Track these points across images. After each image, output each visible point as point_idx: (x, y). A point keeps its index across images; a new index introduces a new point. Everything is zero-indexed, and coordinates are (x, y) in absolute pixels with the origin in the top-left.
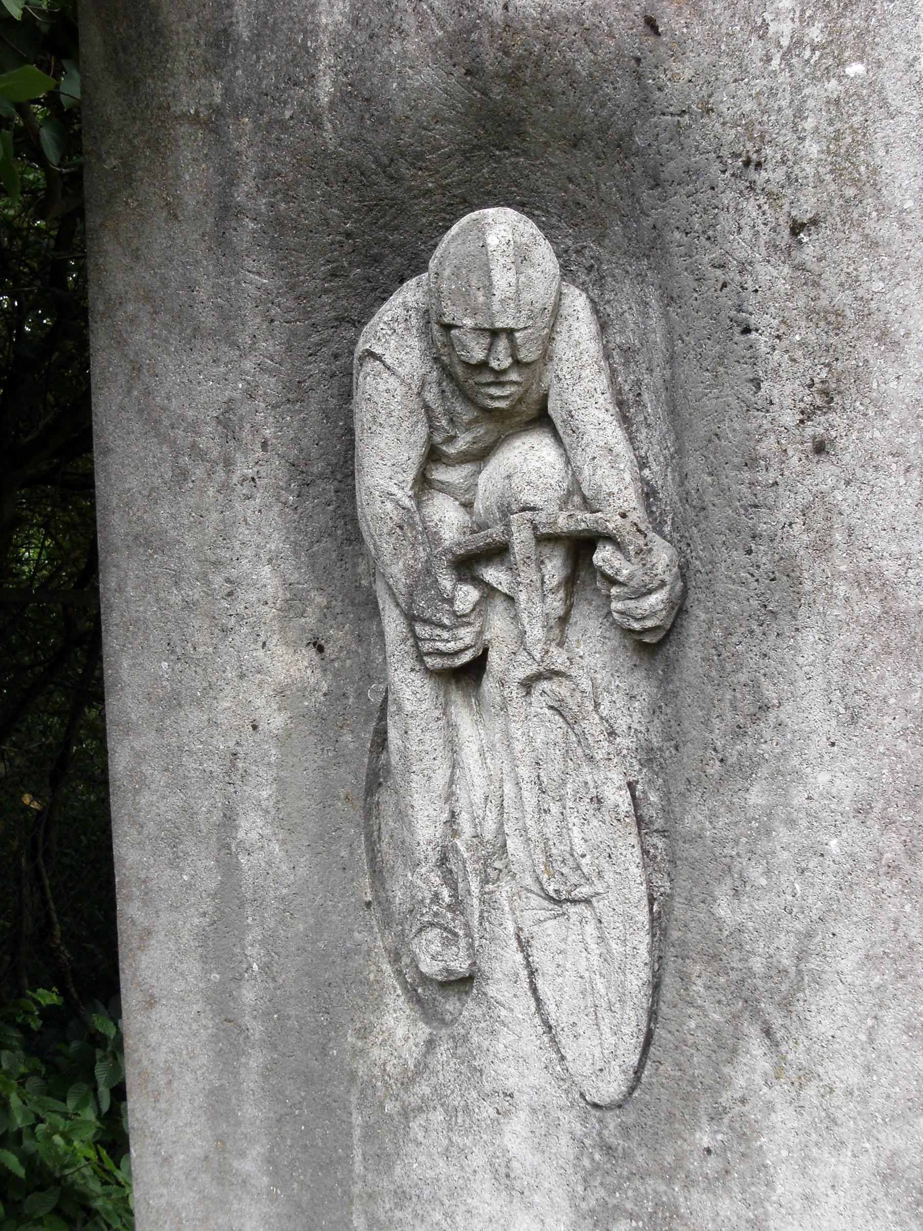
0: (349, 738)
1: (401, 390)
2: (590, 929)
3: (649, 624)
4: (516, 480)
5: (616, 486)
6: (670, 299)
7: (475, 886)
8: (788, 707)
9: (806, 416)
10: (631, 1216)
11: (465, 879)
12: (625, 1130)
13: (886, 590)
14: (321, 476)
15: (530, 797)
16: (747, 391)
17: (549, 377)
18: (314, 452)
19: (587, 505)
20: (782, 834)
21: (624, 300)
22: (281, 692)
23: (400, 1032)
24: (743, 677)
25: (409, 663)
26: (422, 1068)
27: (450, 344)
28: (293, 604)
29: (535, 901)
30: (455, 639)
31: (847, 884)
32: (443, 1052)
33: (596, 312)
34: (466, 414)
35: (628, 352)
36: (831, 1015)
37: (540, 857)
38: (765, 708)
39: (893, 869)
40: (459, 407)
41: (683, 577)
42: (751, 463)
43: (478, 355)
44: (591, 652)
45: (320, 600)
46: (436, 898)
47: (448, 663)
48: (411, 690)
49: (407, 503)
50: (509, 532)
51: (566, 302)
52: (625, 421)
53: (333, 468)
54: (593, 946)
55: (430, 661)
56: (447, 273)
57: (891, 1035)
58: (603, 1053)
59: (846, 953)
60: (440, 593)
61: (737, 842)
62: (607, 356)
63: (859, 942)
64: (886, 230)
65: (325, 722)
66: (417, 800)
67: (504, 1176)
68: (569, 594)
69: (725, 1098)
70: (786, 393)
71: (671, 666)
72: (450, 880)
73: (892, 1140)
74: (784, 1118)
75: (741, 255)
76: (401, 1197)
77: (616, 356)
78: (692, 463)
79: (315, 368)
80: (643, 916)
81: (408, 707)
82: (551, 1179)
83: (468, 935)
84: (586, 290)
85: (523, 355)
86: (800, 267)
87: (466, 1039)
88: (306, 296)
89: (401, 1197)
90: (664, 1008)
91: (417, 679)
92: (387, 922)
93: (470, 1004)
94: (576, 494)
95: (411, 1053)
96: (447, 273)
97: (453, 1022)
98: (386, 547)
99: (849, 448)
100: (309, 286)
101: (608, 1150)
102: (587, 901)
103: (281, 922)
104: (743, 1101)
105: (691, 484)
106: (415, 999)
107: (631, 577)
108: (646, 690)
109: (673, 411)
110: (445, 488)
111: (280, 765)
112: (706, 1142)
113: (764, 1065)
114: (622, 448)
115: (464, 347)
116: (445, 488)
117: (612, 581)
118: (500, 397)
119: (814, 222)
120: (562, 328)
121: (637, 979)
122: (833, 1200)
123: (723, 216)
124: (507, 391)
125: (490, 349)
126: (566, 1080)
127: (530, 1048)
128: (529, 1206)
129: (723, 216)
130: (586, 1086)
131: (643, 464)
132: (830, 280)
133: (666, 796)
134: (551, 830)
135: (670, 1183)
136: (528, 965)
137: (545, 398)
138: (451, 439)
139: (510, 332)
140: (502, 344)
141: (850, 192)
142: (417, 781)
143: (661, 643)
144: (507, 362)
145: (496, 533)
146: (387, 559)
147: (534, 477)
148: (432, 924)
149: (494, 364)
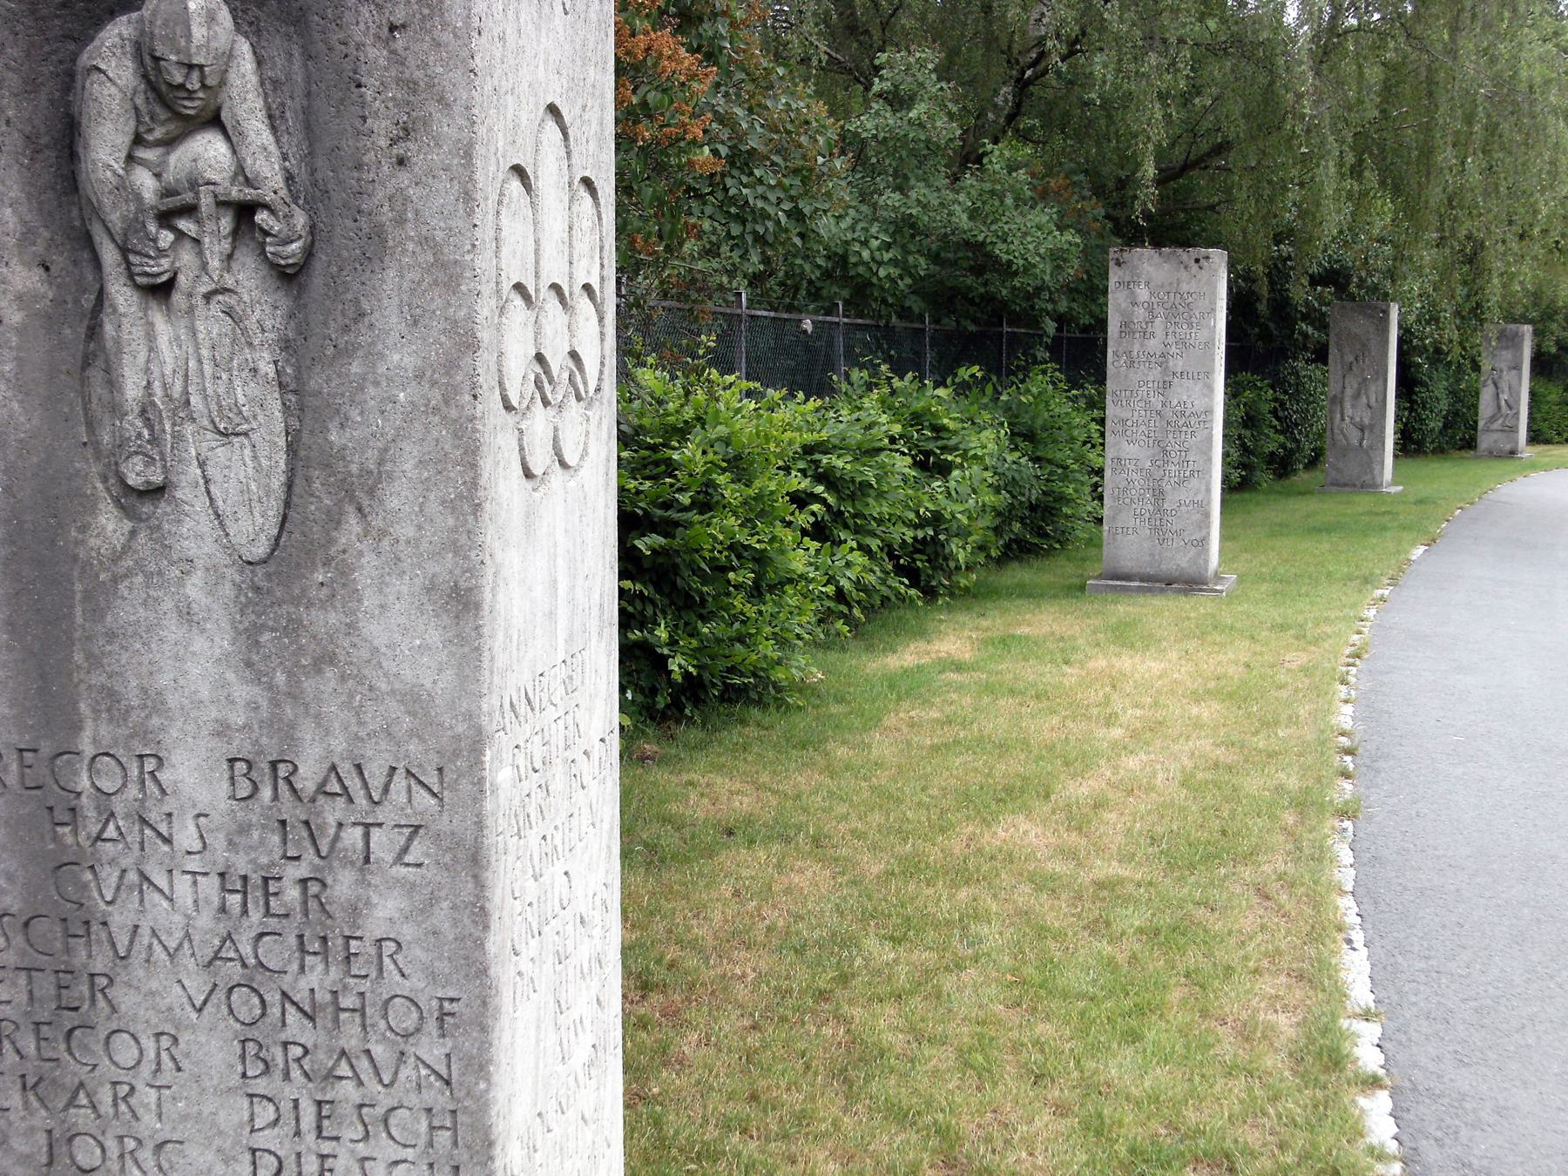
0: (68, 331)
1: (119, 96)
2: (247, 452)
3: (290, 261)
4: (200, 164)
5: (269, 171)
6: (308, 56)
7: (168, 427)
8: (376, 315)
9: (394, 142)
10: (273, 630)
11: (161, 422)
12: (269, 576)
13: (436, 249)
14: (47, 146)
15: (208, 368)
16: (358, 123)
17: (223, 96)
18: (43, 129)
19: (248, 182)
20: (371, 391)
21: (275, 48)
22: (19, 298)
23: (110, 527)
24: (349, 296)
25: (123, 280)
26: (126, 548)
27: (158, 70)
28: (28, 236)
29: (209, 435)
30: (159, 265)
31: (408, 419)
32: (142, 537)
33: (255, 53)
34: (163, 114)
35: (276, 83)
36: (398, 497)
37: (214, 407)
38: (362, 315)
39: (436, 410)
40: (158, 109)
41: (312, 233)
42: (359, 167)
43: (178, 78)
44: (248, 278)
45: (46, 234)
46: (139, 435)
47: (151, 281)
48: (122, 296)
49: (121, 172)
50: (198, 199)
51: (236, 46)
52: (274, 129)
53: (63, 141)
54: (249, 462)
55: (139, 280)
56: (159, 23)
57: (433, 507)
58: (254, 529)
59: (407, 463)
60: (147, 234)
61: (343, 395)
62: (262, 84)
63: (415, 453)
64: (446, 37)
65: (51, 319)
66: (127, 372)
67: (186, 615)
68: (234, 240)
69: (333, 551)
70: (382, 127)
71: (302, 289)
72: (148, 423)
73: (433, 568)
74: (369, 560)
75: (358, 39)
76: (111, 636)
77: (270, 86)
78: (320, 162)
79: (46, 69)
80: (282, 442)
81: (122, 309)
82: (219, 612)
83: (163, 459)
84: (247, 37)
85: (209, 82)
86: (394, 52)
87: (159, 527)
88: (43, 18)
89: (111, 636)
90: (295, 499)
91: (128, 291)
92: (98, 455)
93: (163, 504)
94: (241, 174)
95: (118, 541)
96: (159, 23)
97: (148, 519)
98: (107, 201)
99: (418, 162)
100: (45, 12)
101: (257, 589)
102: (246, 434)
103: (20, 456)
104: (344, 552)
105: (319, 176)
106: (117, 501)
107: (280, 231)
108: (285, 303)
109: (308, 128)
110: (143, 163)
111: (19, 349)
112: (321, 578)
113: (358, 529)
114: (273, 148)
115: (169, 73)
116: (143, 163)
117: (267, 233)
118: (190, 108)
119: (404, 26)
120: (234, 64)
121: (277, 482)
122: (398, 606)
123: (347, 13)
124: (197, 103)
125: (187, 76)
126: (230, 548)
127: (206, 529)
128: (203, 631)
129: (347, 13)
130: (243, 551)
131: (285, 158)
132: (411, 62)
133: (298, 369)
134: (221, 390)
135: (297, 606)
136: (204, 477)
137: (219, 109)
138: (150, 130)
139: (201, 67)
140: (195, 75)
141: (426, 11)
142: (126, 359)
143: (295, 275)
144: (197, 86)
145: (188, 197)
146: (107, 210)
147: (213, 162)
148: (136, 453)
149: (189, 86)
